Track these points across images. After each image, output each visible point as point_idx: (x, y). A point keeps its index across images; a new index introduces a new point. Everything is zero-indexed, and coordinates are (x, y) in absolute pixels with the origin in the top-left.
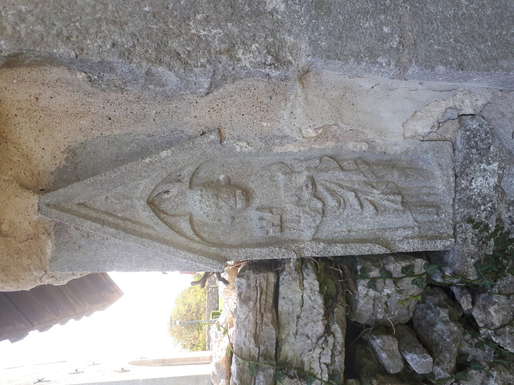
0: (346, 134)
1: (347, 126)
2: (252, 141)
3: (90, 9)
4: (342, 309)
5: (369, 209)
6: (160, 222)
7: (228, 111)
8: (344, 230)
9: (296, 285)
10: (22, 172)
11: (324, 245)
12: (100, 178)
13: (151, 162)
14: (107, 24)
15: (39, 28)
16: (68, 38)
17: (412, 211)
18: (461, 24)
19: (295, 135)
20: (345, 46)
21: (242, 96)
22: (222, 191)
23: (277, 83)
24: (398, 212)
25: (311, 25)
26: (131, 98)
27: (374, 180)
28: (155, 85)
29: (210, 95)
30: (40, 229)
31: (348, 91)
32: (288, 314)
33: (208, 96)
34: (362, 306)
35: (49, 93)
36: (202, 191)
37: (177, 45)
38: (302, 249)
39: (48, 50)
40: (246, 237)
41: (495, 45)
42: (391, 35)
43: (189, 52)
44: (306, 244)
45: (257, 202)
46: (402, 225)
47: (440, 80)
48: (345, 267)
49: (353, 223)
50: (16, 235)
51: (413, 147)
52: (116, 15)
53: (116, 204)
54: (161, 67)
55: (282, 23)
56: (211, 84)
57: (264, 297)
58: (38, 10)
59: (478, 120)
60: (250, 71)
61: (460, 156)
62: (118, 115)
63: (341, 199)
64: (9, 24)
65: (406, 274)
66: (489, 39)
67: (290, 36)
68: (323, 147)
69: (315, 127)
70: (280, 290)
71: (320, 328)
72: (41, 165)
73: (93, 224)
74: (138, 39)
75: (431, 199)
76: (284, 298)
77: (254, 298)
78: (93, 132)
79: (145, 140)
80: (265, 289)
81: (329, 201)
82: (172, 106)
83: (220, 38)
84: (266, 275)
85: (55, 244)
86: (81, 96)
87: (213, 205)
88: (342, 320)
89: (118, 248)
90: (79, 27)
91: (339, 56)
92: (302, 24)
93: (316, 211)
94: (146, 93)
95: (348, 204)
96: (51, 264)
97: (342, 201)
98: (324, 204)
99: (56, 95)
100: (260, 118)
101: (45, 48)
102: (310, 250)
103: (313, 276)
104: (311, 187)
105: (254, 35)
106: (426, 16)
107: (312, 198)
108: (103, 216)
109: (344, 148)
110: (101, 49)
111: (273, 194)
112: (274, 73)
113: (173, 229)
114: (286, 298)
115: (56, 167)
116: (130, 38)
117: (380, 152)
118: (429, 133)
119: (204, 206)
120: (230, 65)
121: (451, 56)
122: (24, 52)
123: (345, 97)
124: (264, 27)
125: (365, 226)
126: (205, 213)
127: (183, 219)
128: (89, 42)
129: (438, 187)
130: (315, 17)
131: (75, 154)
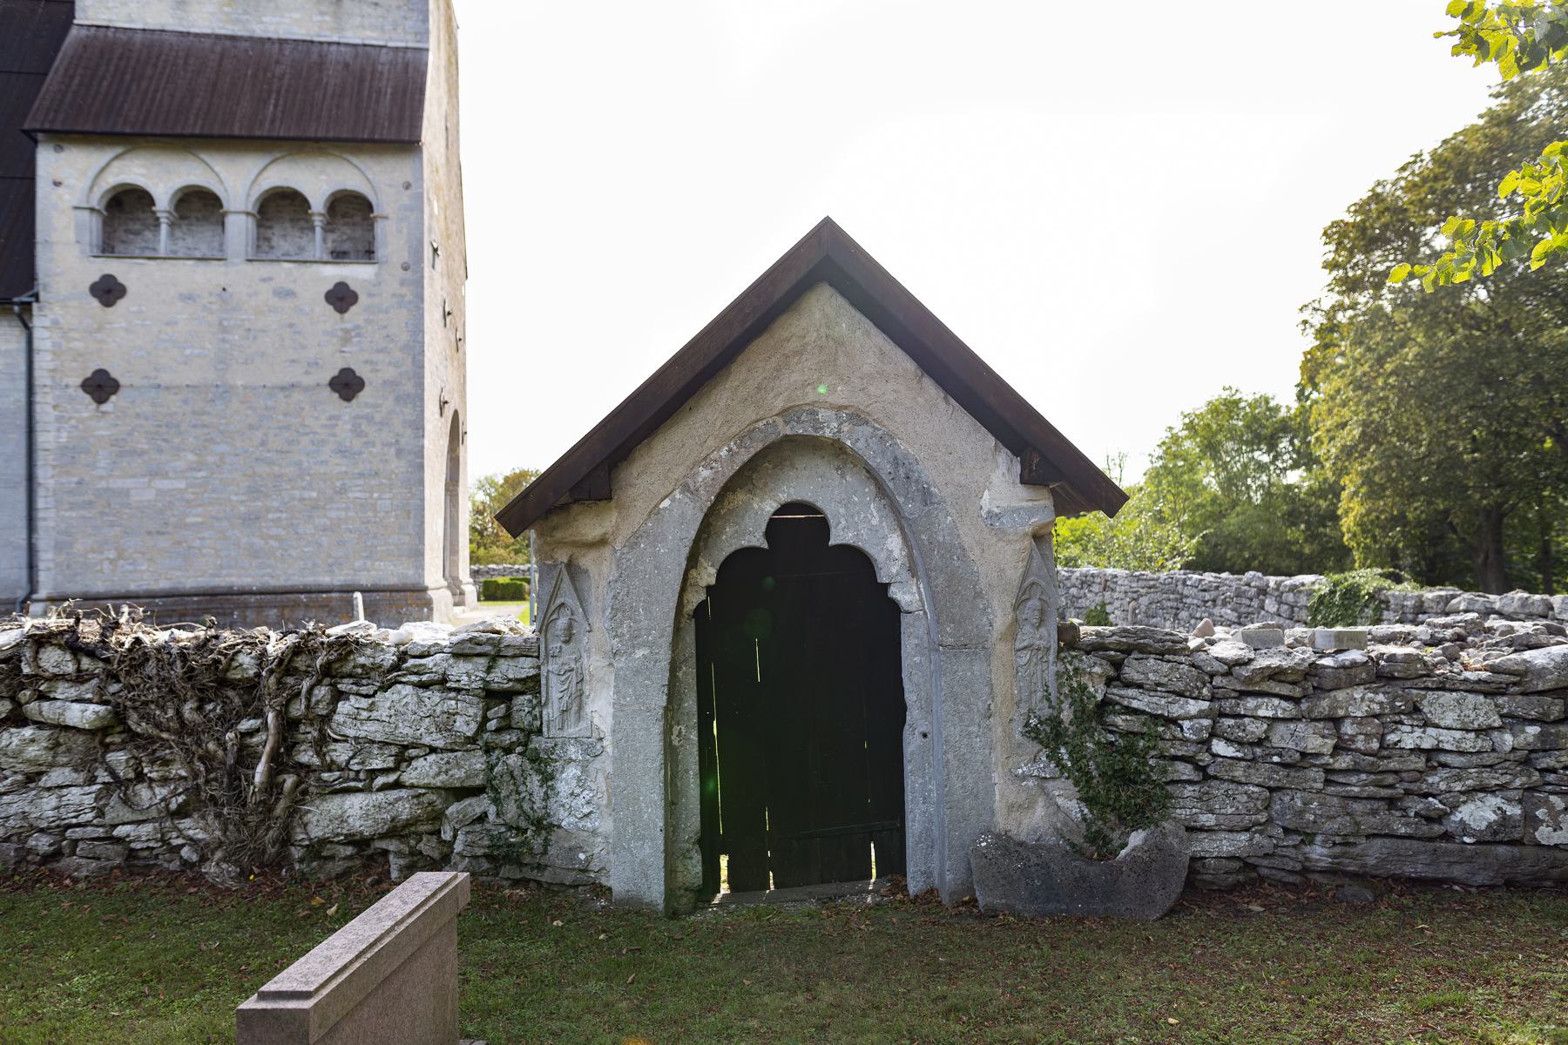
5: (561, 695)
71: (511, 676)
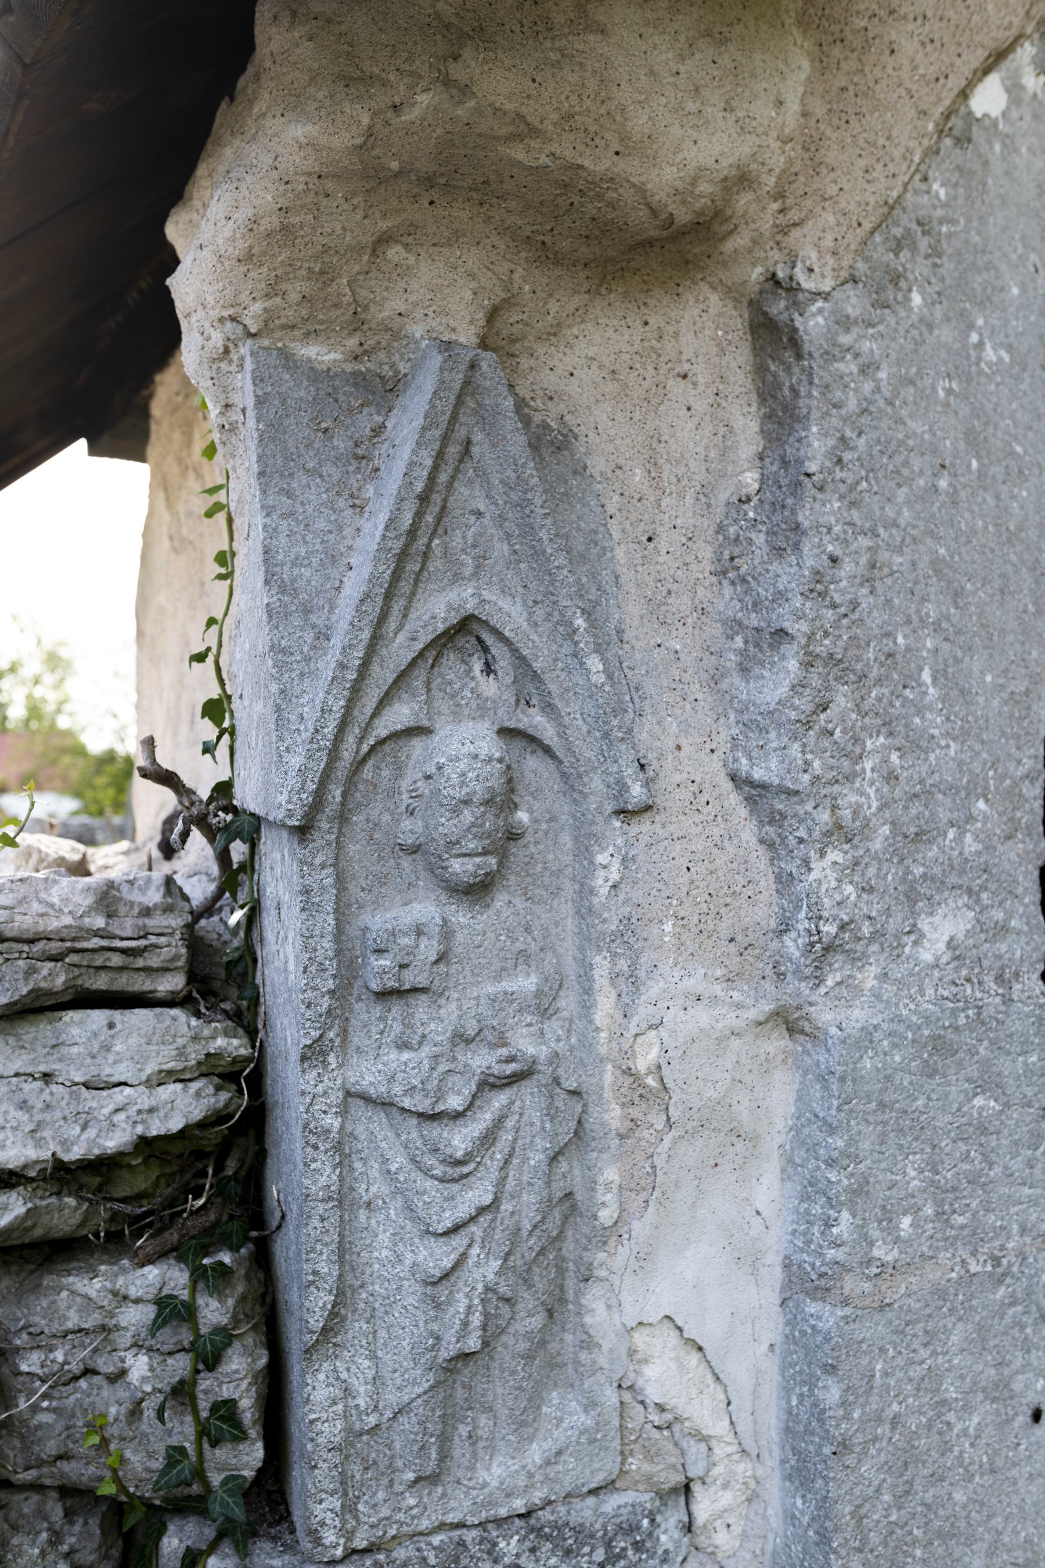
0: (640, 1156)
1: (664, 1156)
2: (621, 897)
3: (892, 515)
4: (72, 1221)
6: (419, 646)
7: (694, 830)
8: (373, 1189)
9: (164, 1058)
10: (524, 317)
11: (335, 1130)
12: (539, 502)
13: (575, 631)
14: (869, 549)
15: (852, 405)
16: (840, 461)
17: (431, 1394)
18: (929, 1427)
19: (643, 1013)
20: (867, 1121)
21: (734, 866)
22: (497, 816)
23: (768, 953)
24: (433, 1346)
25: (901, 1028)
26: (701, 592)
27: (523, 1256)
28: (743, 653)
29: (729, 785)
30: (376, 337)
31: (750, 1145)
32: (54, 1042)
33: (728, 779)
34: (73, 1293)
35: (700, 406)
36: (500, 761)
37: (843, 704)
38: (323, 1062)
39: (815, 414)
40: (359, 890)
41: (892, 1532)
42: (897, 1240)
43: (832, 734)
44: (336, 1073)
45: (461, 917)
46: (385, 1372)
47: (789, 1402)
48: (212, 1217)
49: (396, 1214)
50: (372, 275)
51: (603, 1361)
52: (886, 571)
53: (464, 537)
54: (797, 665)
55: (898, 956)
56: (764, 786)
57: (116, 960)
58: (881, 403)
59: (678, 1544)
60: (796, 882)
61: (585, 1511)
62: (661, 560)
63: (473, 1165)
64: (856, 341)
65: (208, 1419)
66: (903, 1512)
67: (875, 978)
68: (608, 1094)
69: (664, 1066)
70: (136, 1011)
72: (532, 362)
73: (425, 473)
74: (846, 615)
75: (459, 1450)
76: (111, 1026)
77: (115, 929)
78: (616, 498)
79: (607, 620)
80: (140, 963)
81: (464, 1131)
82: (695, 690)
83: (862, 806)
84: (180, 964)
85: (329, 369)
86: (697, 477)
87: (465, 790)
88: (34, 1226)
89: (330, 532)
90: (859, 488)
91: (846, 1107)
92: (901, 1005)
93: (440, 1095)
94: (717, 630)
95: (456, 1187)
96: (275, 352)
97: (466, 1170)
98: (458, 1116)
99: (696, 420)
100: (681, 914)
101: (818, 408)
102: (320, 1088)
103: (196, 1112)
104: (508, 1072)
105: (871, 890)
106: (941, 1324)
107: (476, 1078)
108: (437, 498)
109: (605, 1156)
110: (825, 530)
111: (483, 961)
112: (792, 946)
113: (395, 682)
114: (112, 1032)
115: (528, 397)
116: (848, 597)
117: (591, 1264)
118: (642, 1402)
119: (462, 766)
120: (810, 831)
121: (863, 1413)
122: (806, 363)
123: (735, 1140)
124: (888, 912)
125: (385, 1253)
126: (439, 768)
127: (421, 708)
128: (837, 505)
129: (495, 1464)
130: (917, 1037)
131: (559, 448)
